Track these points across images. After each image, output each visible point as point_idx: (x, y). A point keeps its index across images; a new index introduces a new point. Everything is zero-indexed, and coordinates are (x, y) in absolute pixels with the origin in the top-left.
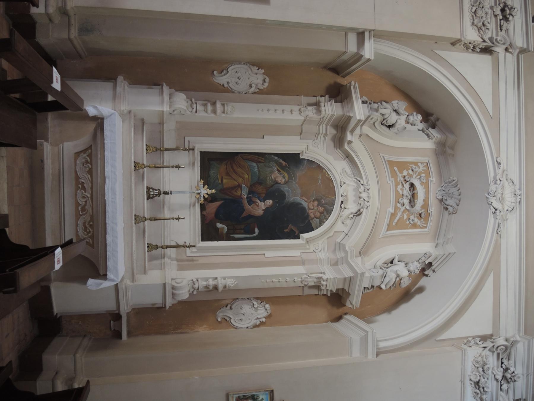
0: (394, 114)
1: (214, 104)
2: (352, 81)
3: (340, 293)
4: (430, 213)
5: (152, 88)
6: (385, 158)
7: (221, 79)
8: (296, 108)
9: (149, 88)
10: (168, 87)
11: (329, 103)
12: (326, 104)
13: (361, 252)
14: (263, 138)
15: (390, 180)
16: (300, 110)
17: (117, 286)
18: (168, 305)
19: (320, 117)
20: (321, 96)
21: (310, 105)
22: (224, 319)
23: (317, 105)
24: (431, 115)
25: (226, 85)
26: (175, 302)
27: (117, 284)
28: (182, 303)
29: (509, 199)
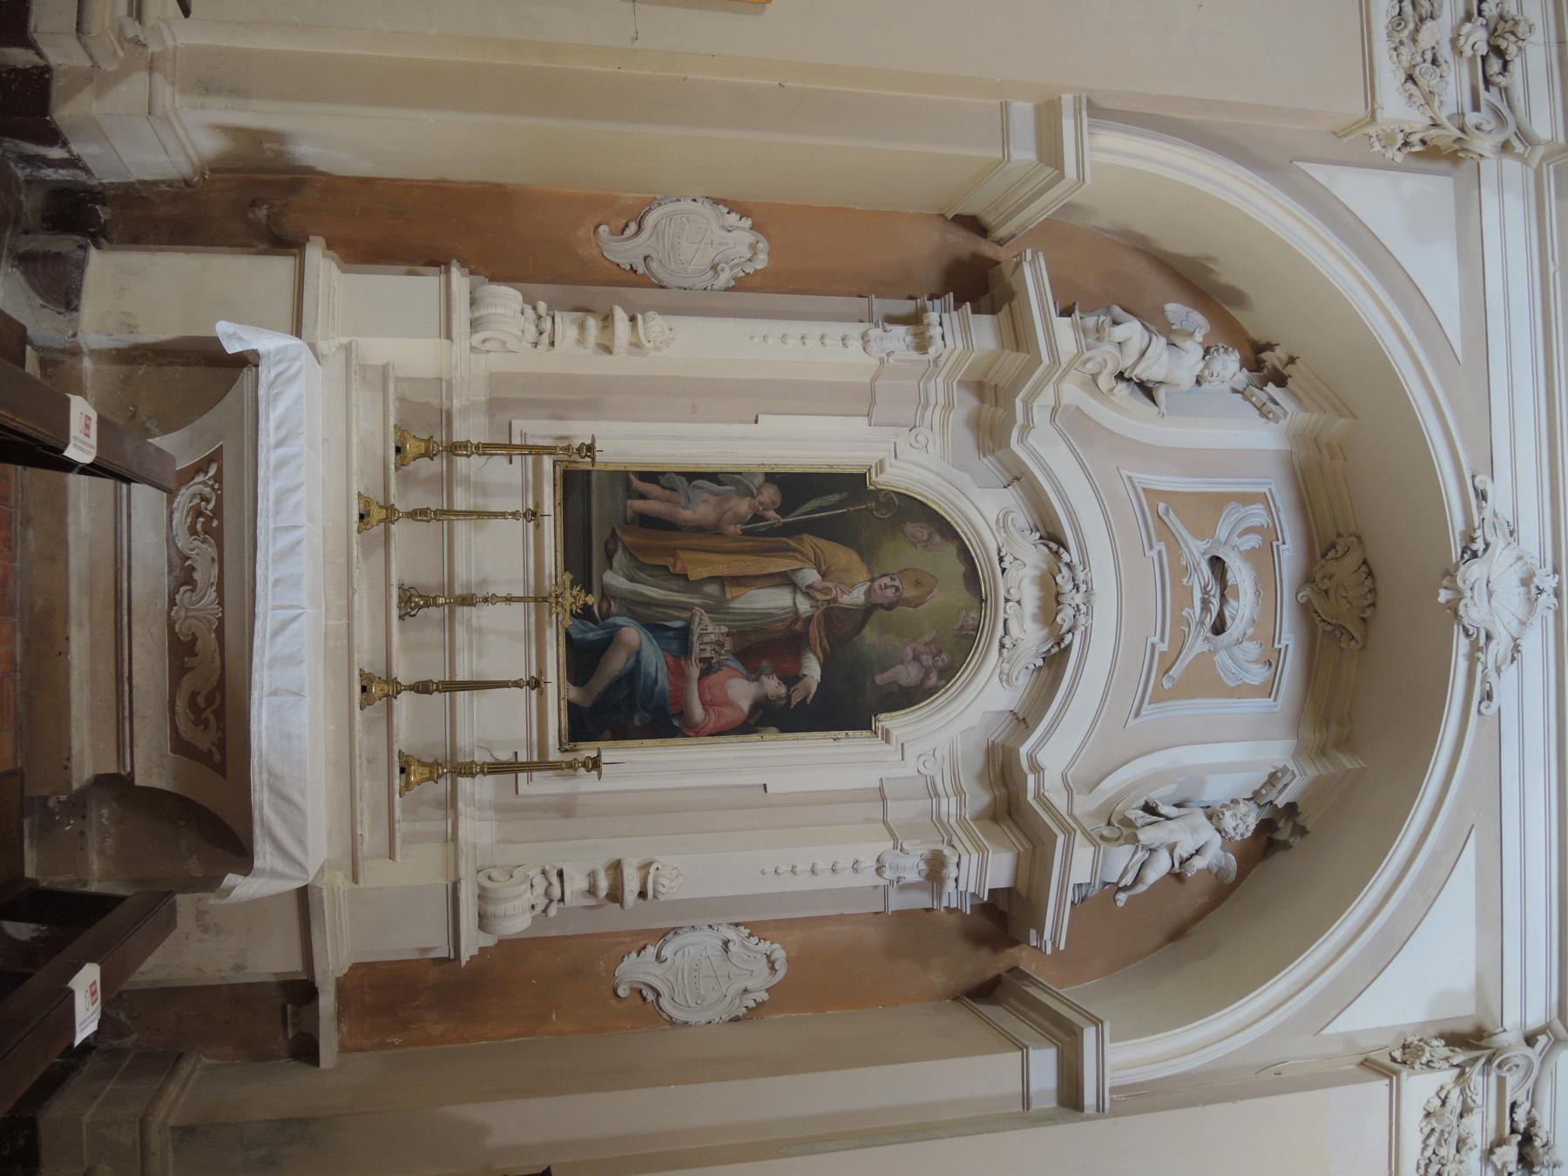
0: (427, 576)
1: (607, 320)
2: (1025, 251)
3: (1002, 905)
4: (1280, 650)
5: (418, 274)
6: (1136, 481)
7: (624, 252)
8: (855, 330)
9: (410, 273)
10: (458, 264)
11: (954, 313)
12: (945, 317)
13: (1069, 774)
14: (756, 422)
15: (1151, 547)
16: (864, 336)
17: (303, 894)
18: (467, 952)
19: (925, 357)
20: (931, 298)
21: (892, 320)
22: (638, 995)
23: (914, 320)
24: (1269, 347)
25: (641, 270)
26: (489, 941)
27: (305, 888)
28: (511, 948)
29: (1510, 596)
